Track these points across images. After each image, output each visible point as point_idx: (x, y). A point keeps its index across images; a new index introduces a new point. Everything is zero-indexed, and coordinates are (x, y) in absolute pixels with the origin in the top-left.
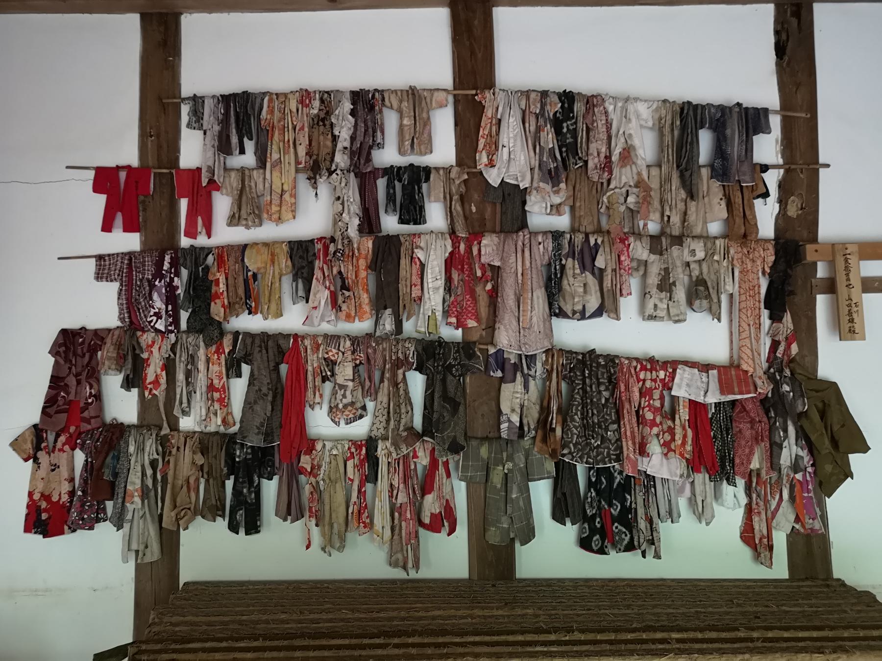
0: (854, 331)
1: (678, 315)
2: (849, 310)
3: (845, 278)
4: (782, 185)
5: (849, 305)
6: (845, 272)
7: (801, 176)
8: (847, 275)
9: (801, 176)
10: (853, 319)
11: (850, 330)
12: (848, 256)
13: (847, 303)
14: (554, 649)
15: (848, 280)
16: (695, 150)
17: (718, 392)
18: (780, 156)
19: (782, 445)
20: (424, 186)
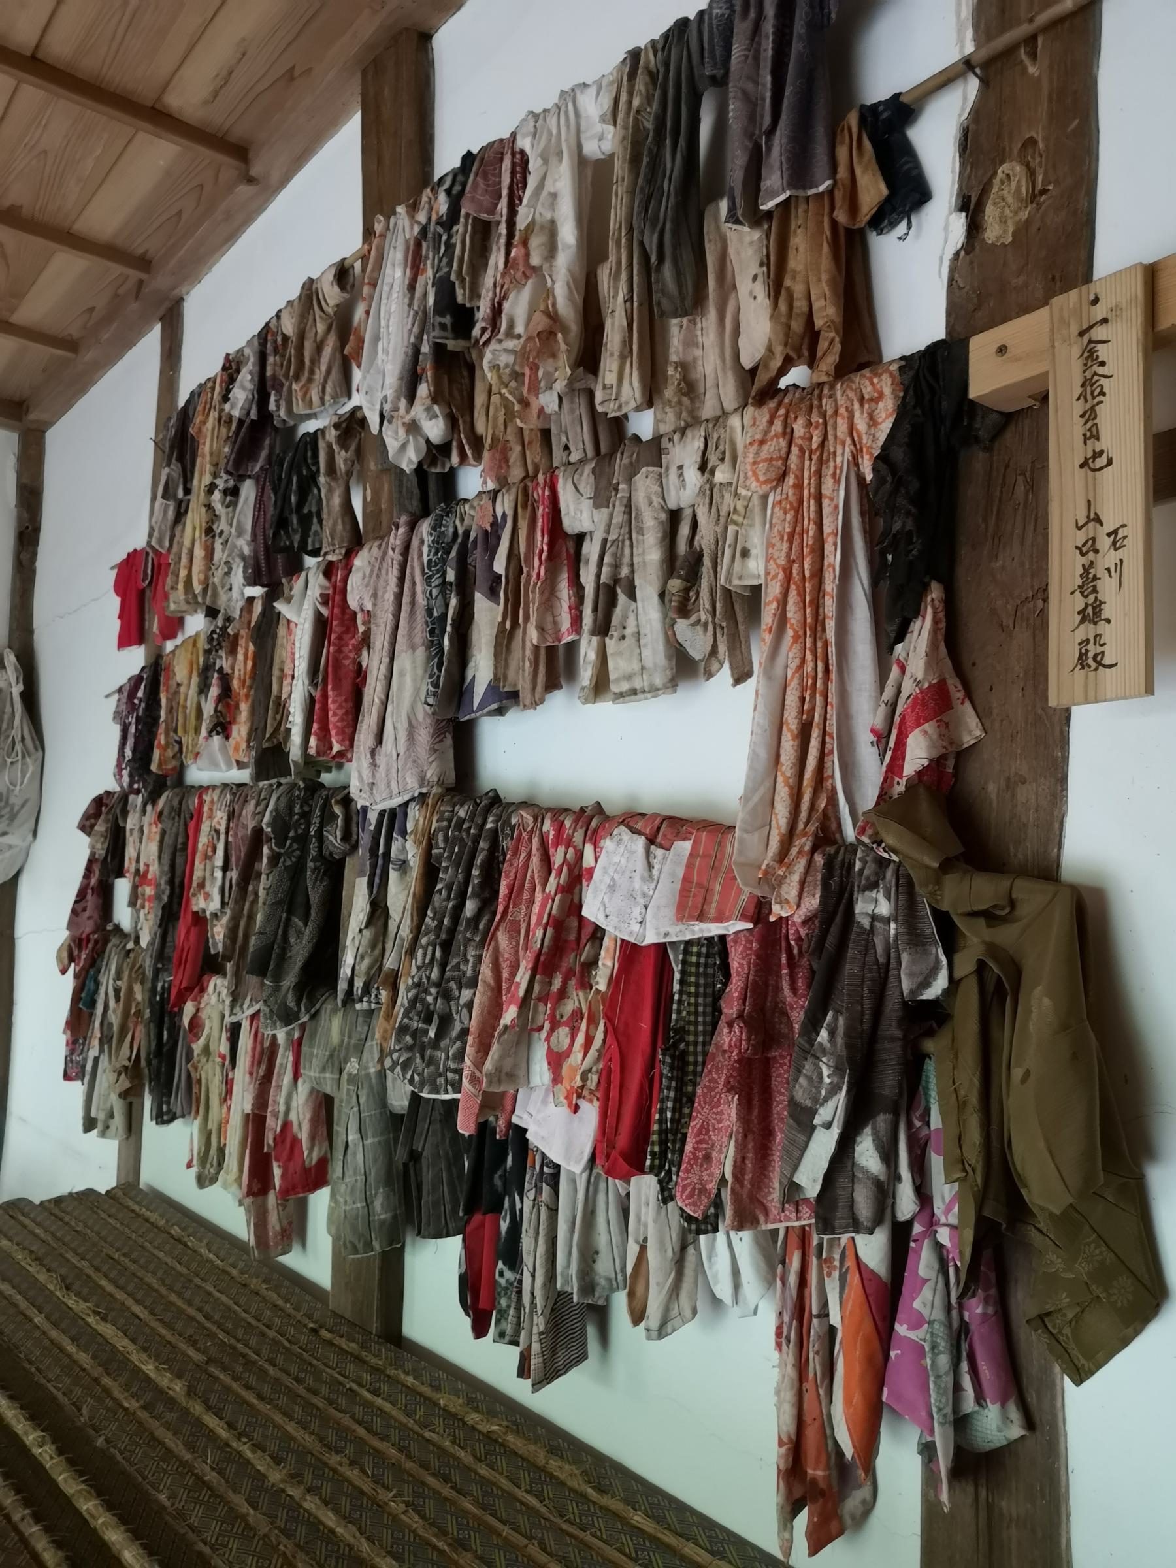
0: (1099, 660)
1: (629, 677)
2: (1086, 570)
3: (1079, 429)
4: (974, 145)
5: (1089, 547)
6: (1079, 408)
7: (1032, 70)
8: (1090, 415)
9: (1032, 70)
10: (1098, 607)
11: (1082, 656)
12: (1099, 333)
13: (1081, 537)
14: (243, 923)
15: (1092, 434)
16: (225, 248)
17: (670, 912)
18: (969, 33)
19: (813, 1113)
20: (584, 883)
